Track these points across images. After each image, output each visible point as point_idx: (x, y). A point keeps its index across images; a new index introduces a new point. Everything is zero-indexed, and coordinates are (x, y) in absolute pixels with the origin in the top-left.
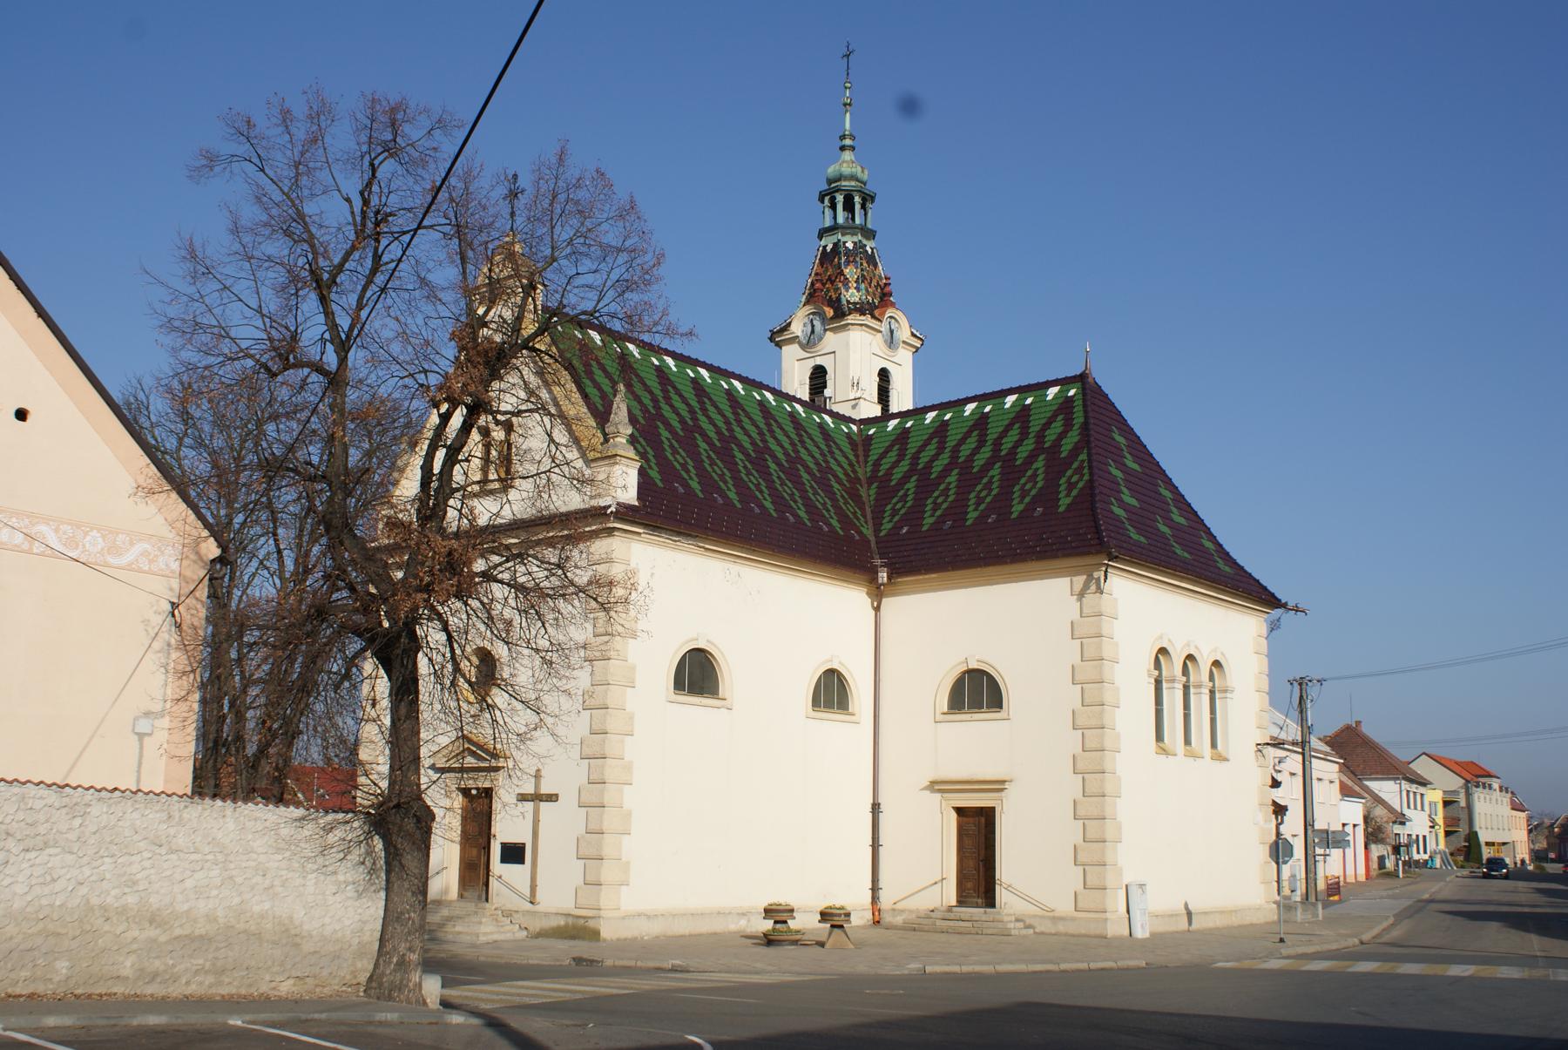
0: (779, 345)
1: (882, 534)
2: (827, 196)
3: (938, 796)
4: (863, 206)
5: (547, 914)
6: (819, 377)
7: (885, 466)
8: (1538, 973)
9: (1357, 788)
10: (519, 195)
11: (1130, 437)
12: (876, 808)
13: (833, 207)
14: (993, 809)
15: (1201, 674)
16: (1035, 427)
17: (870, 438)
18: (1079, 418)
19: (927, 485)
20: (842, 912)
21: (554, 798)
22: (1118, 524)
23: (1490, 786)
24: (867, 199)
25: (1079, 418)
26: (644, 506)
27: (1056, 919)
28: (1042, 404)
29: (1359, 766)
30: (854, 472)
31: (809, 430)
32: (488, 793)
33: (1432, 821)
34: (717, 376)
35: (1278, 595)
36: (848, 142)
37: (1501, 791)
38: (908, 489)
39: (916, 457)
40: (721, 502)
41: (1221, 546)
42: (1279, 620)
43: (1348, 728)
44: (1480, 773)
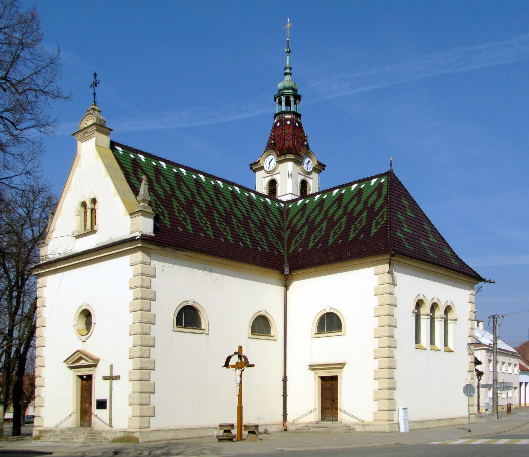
0: (255, 171)
1: (290, 252)
3: (313, 372)
4: (295, 103)
5: (116, 432)
6: (273, 184)
10: (97, 84)
11: (411, 201)
12: (285, 379)
13: (280, 103)
15: (439, 312)
16: (364, 198)
17: (289, 209)
18: (385, 192)
19: (312, 228)
21: (118, 378)
24: (298, 98)
25: (385, 192)
27: (365, 425)
31: (257, 205)
32: (90, 378)
34: (243, 190)
35: (481, 275)
36: (288, 71)
38: (304, 231)
39: (308, 216)
40: (203, 236)
41: (454, 253)
42: (481, 287)
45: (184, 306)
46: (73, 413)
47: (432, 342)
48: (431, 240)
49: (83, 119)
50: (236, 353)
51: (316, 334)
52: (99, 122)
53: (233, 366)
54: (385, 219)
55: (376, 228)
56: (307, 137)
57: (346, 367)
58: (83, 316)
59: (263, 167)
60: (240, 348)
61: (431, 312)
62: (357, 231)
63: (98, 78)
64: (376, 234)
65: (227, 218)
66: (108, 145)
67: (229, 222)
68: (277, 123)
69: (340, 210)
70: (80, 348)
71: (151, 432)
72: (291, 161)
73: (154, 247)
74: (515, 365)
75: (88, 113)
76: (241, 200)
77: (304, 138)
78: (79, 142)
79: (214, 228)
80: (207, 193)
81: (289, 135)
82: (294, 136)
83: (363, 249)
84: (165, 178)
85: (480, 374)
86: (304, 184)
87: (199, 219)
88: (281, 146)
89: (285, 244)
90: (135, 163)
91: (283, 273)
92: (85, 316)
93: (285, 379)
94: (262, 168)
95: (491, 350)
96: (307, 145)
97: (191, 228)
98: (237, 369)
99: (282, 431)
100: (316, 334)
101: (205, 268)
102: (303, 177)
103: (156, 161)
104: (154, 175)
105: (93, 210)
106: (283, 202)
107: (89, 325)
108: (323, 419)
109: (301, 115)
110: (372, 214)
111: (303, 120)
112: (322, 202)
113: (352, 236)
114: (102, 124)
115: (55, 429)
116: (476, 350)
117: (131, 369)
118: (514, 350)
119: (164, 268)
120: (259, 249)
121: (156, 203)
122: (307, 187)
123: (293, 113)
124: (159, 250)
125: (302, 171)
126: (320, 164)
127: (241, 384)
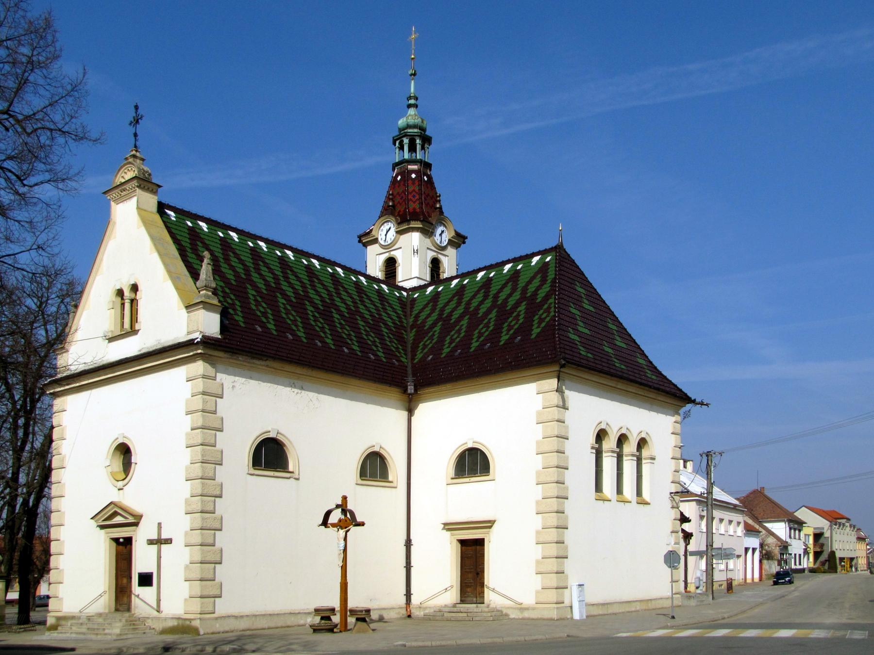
0: (365, 245)
1: (416, 361)
2: (398, 140)
3: (449, 533)
4: (423, 148)
5: (166, 619)
6: (391, 264)
8: (839, 634)
9: (757, 527)
10: (140, 120)
11: (589, 289)
12: (408, 544)
13: (401, 148)
15: (630, 448)
17: (414, 300)
18: (551, 275)
21: (169, 542)
22: (573, 345)
23: (844, 525)
25: (551, 275)
26: (224, 339)
27: (522, 609)
29: (760, 514)
30: (401, 322)
32: (128, 541)
33: (806, 545)
35: (689, 395)
36: (412, 102)
38: (435, 331)
40: (291, 338)
41: (651, 362)
42: (689, 411)
43: (755, 492)
46: (105, 592)
47: (619, 491)
49: (122, 167)
50: (338, 506)
51: (452, 479)
52: (142, 175)
53: (334, 525)
54: (552, 314)
56: (440, 196)
59: (377, 239)
60: (345, 498)
61: (617, 447)
62: (511, 332)
63: (140, 111)
64: (539, 335)
65: (352, 318)
66: (154, 208)
71: (216, 619)
72: (418, 231)
73: (221, 354)
74: (739, 523)
75: (126, 162)
77: (435, 198)
78: (113, 204)
85: (687, 536)
86: (435, 264)
88: (403, 209)
89: (409, 349)
90: (194, 233)
91: (405, 391)
92: (121, 453)
93: (408, 544)
94: (375, 241)
96: (441, 208)
99: (404, 618)
101: (294, 383)
102: (435, 254)
105: (133, 301)
108: (463, 601)
110: (533, 306)
111: (434, 173)
113: (504, 338)
114: (146, 178)
118: (736, 502)
119: (235, 384)
120: (372, 356)
123: (420, 162)
124: (228, 358)
126: (458, 235)
127: (345, 550)
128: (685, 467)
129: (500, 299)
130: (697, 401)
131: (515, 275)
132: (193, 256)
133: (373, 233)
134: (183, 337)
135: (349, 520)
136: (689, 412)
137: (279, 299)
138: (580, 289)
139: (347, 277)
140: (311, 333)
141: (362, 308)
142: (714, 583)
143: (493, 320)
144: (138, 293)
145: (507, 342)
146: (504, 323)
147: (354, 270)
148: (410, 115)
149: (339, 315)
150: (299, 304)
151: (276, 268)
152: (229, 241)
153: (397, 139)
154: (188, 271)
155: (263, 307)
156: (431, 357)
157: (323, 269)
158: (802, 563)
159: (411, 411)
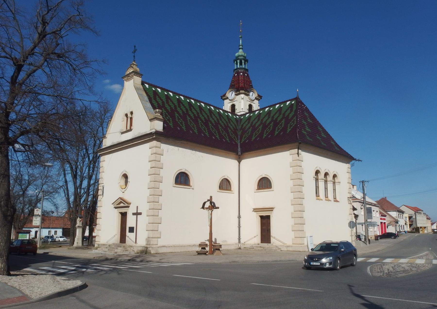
0: (224, 100)
3: (255, 213)
4: (245, 64)
5: (138, 247)
6: (233, 106)
7: (244, 126)
10: (136, 51)
12: (239, 217)
13: (237, 64)
14: (270, 215)
15: (330, 178)
20: (219, 245)
23: (421, 213)
28: (286, 106)
30: (236, 127)
35: (353, 157)
37: (424, 214)
40: (225, 141)
42: (354, 163)
43: (383, 198)
44: (418, 210)
45: (180, 172)
46: (116, 235)
47: (326, 196)
48: (323, 135)
49: (128, 69)
50: (208, 200)
51: (256, 190)
53: (207, 208)
54: (295, 123)
55: (290, 128)
56: (251, 81)
57: (274, 210)
58: (124, 177)
59: (228, 97)
60: (211, 197)
61: (325, 177)
62: (279, 130)
63: (136, 48)
64: (290, 131)
65: (206, 123)
66: (140, 83)
67: (207, 126)
68: (235, 74)
69: (269, 119)
70: (121, 196)
71: (159, 247)
74: (377, 211)
75: (130, 66)
76: (214, 113)
77: (250, 82)
78: (125, 82)
79: (199, 129)
80: (205, 113)
81: (242, 80)
82: (245, 81)
83: (283, 140)
84: (183, 105)
85: (356, 216)
86: (250, 106)
87: (178, 120)
88: (238, 86)
89: (239, 137)
90: (155, 93)
91: (237, 154)
92: (125, 177)
94: (227, 98)
95: (363, 202)
96: (252, 86)
97: (185, 128)
98: (209, 210)
100: (256, 190)
102: (250, 102)
103: (178, 96)
104: (165, 99)
105: (131, 118)
106: (238, 115)
107: (126, 182)
109: (248, 70)
110: (288, 121)
111: (249, 73)
112: (259, 114)
113: (276, 133)
115: (106, 243)
116: (353, 202)
117: (148, 209)
118: (375, 203)
120: (224, 140)
121: (165, 114)
122: (252, 108)
123: (244, 69)
125: (250, 100)
126: (259, 96)
128: (353, 188)
129: (274, 118)
130: (357, 159)
131: (280, 109)
132: (154, 101)
133: (227, 95)
134: (149, 132)
135: (213, 206)
136: (354, 164)
137: (199, 121)
138: (306, 114)
139: (215, 110)
140: (211, 134)
141: (211, 119)
142: (369, 236)
143: (272, 126)
144: (133, 115)
145: (277, 135)
146: (276, 127)
147: (218, 108)
148: (240, 52)
149: (201, 121)
150: (196, 119)
151: (187, 106)
152: (191, 103)
153: (235, 61)
154: (152, 106)
155: (181, 121)
156: (248, 141)
157: (206, 107)
158: (405, 229)
159: (239, 162)
